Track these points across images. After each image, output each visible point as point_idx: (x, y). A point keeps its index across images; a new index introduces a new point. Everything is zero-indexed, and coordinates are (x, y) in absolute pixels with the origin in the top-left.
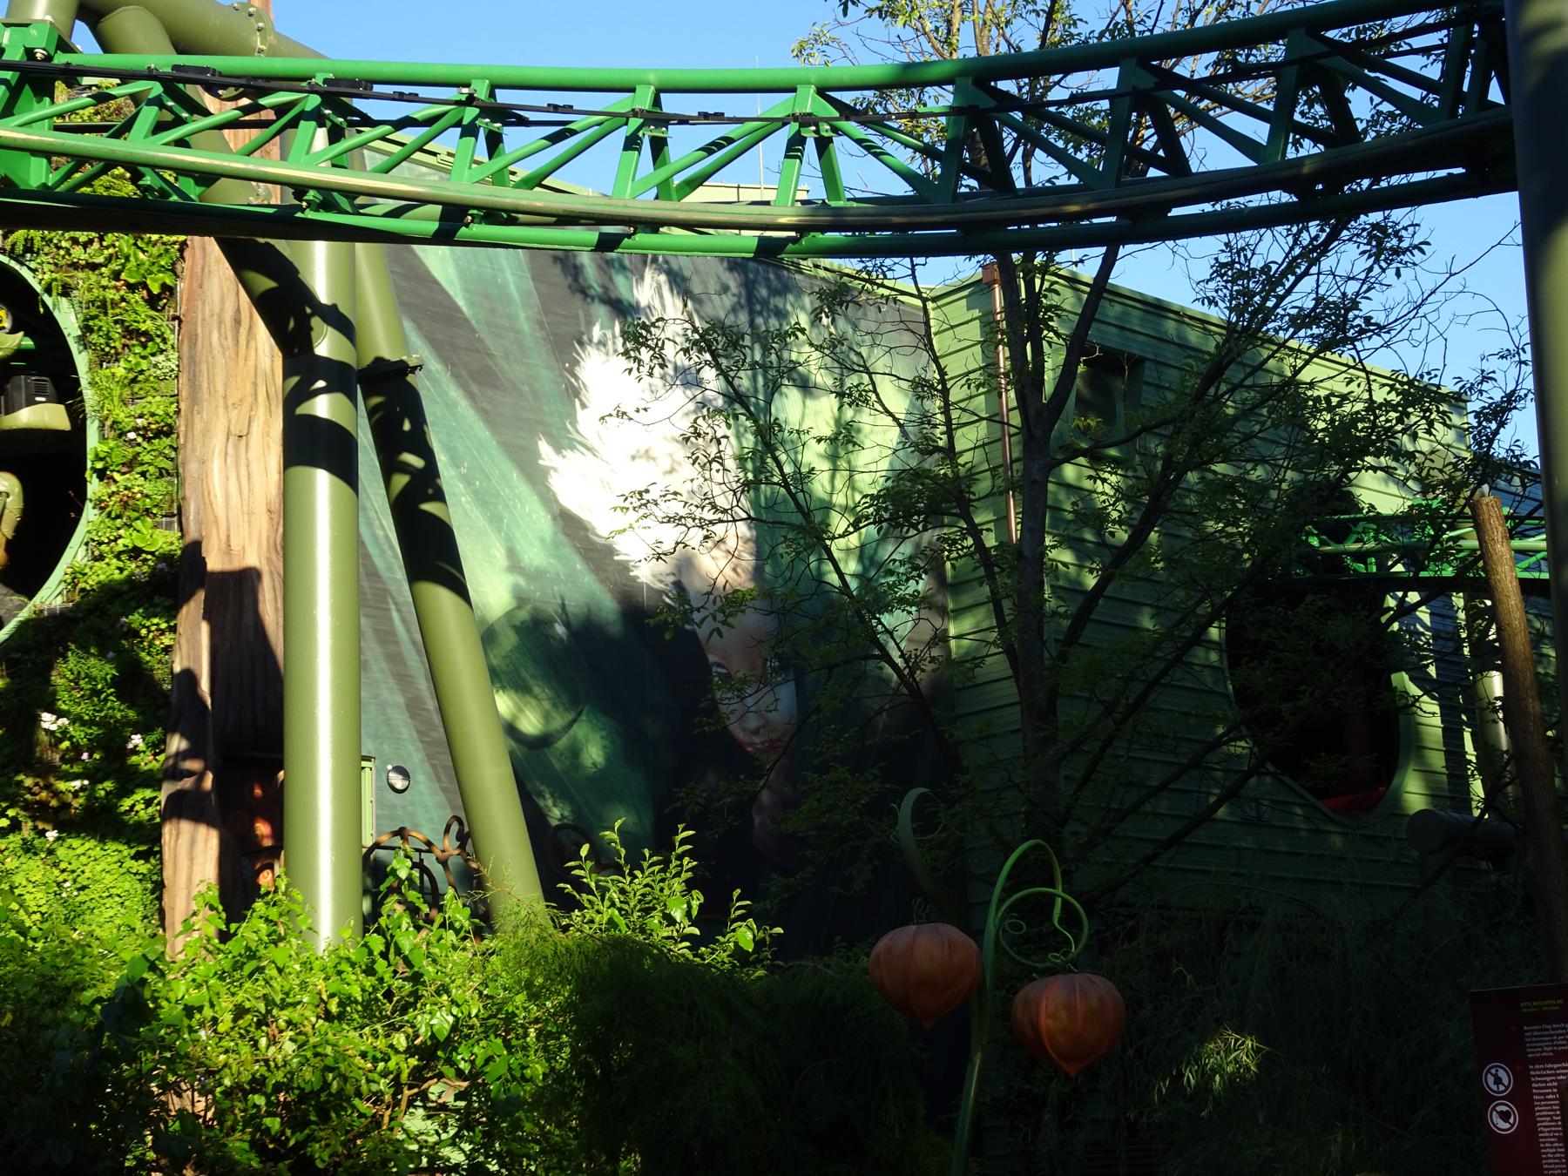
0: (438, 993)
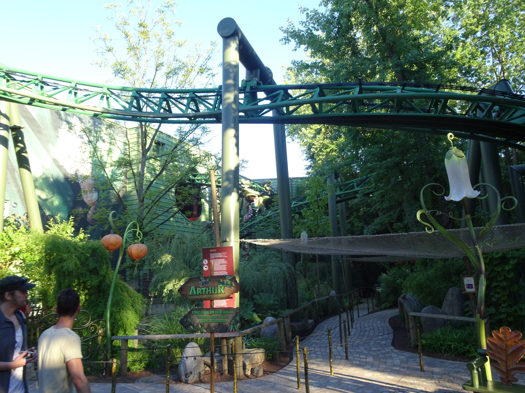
0: (17, 244)
